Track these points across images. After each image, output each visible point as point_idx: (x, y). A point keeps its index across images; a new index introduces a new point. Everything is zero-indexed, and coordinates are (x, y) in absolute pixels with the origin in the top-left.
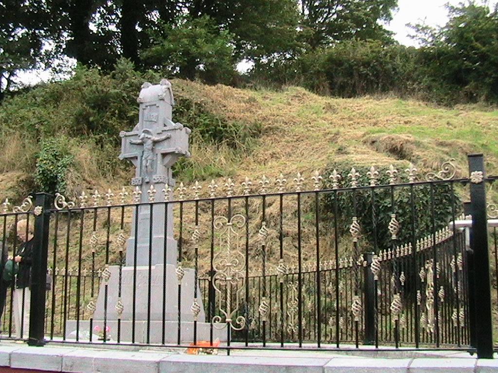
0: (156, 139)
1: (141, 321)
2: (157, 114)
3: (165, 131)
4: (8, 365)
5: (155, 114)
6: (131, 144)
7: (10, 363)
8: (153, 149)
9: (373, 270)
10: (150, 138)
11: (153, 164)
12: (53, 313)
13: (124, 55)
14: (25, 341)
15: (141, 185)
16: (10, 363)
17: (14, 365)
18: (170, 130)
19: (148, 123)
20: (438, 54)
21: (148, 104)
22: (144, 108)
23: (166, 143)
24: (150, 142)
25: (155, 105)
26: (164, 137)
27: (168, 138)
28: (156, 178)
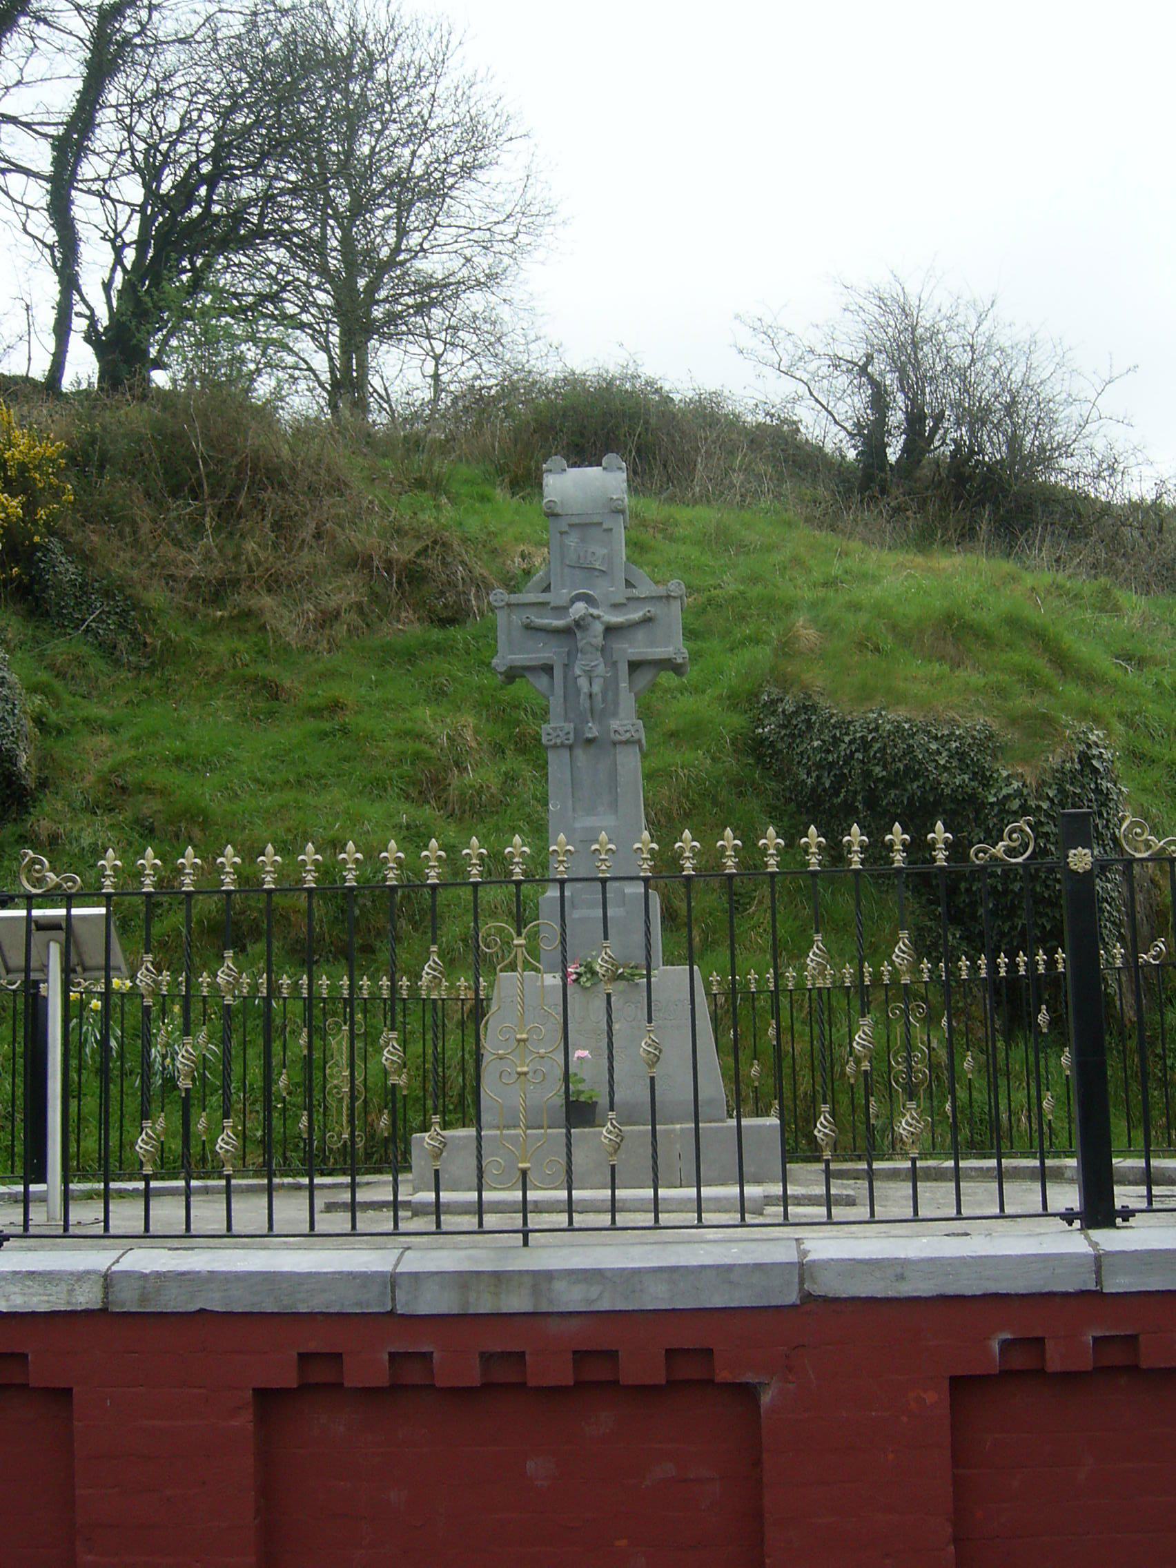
0: (616, 619)
1: (671, 1127)
2: (606, 551)
3: (638, 599)
4: (1092, 1286)
5: (602, 551)
6: (529, 627)
7: (1099, 1281)
8: (603, 650)
9: (898, 960)
10: (599, 617)
11: (611, 685)
12: (122, 1116)
13: (925, 418)
14: (1068, 1217)
15: (571, 747)
16: (1099, 1281)
17: (1117, 1283)
18: (653, 598)
19: (577, 572)
20: (985, 479)
21: (576, 520)
22: (566, 529)
23: (640, 635)
24: (598, 628)
25: (600, 524)
26: (636, 616)
27: (647, 620)
28: (621, 730)
